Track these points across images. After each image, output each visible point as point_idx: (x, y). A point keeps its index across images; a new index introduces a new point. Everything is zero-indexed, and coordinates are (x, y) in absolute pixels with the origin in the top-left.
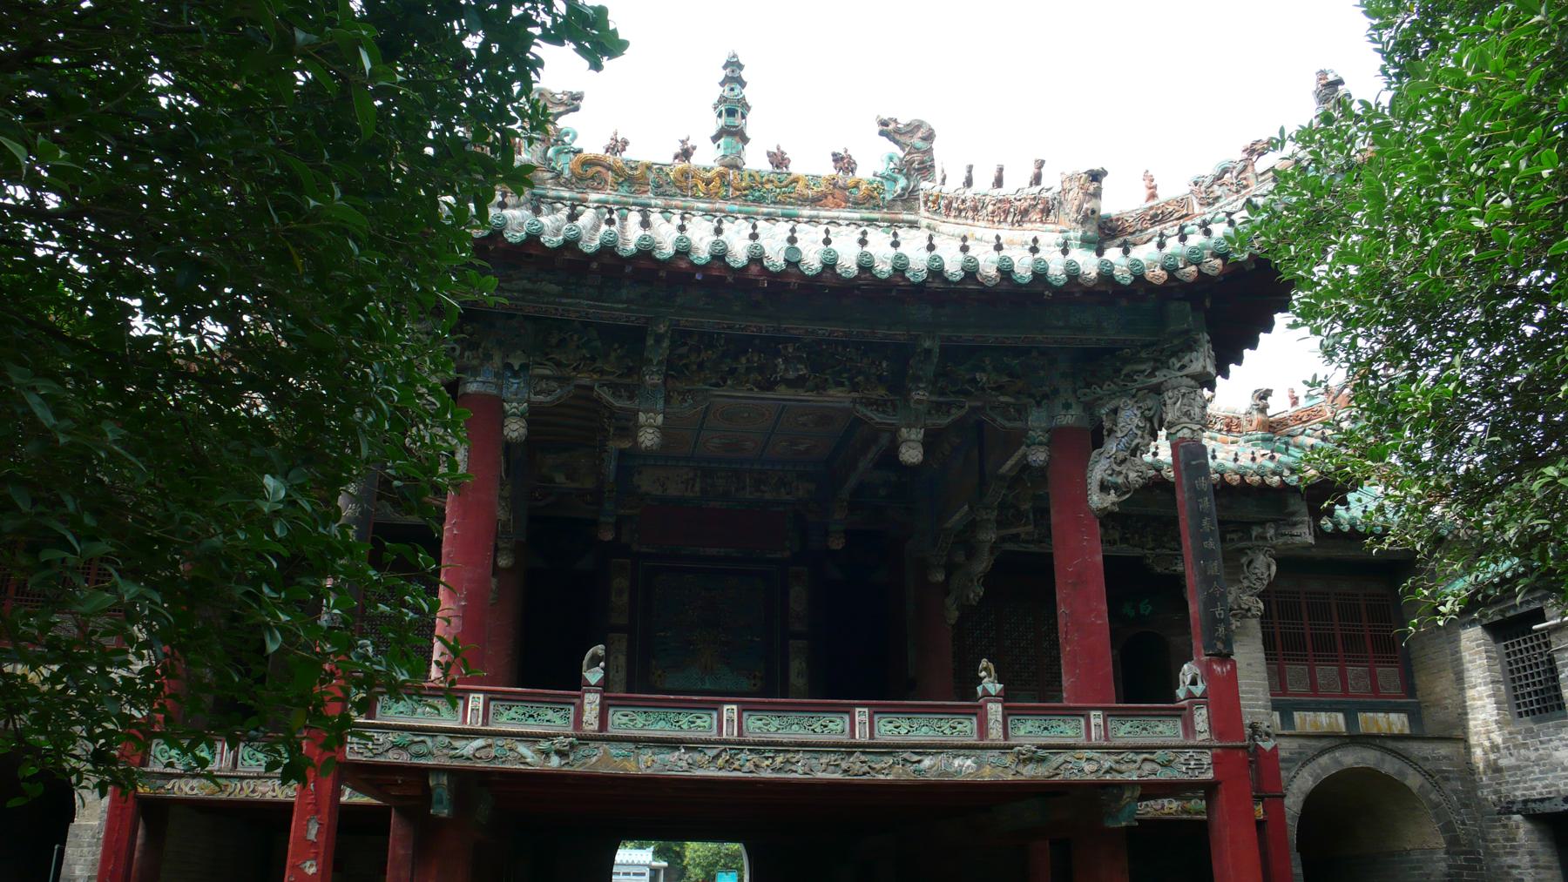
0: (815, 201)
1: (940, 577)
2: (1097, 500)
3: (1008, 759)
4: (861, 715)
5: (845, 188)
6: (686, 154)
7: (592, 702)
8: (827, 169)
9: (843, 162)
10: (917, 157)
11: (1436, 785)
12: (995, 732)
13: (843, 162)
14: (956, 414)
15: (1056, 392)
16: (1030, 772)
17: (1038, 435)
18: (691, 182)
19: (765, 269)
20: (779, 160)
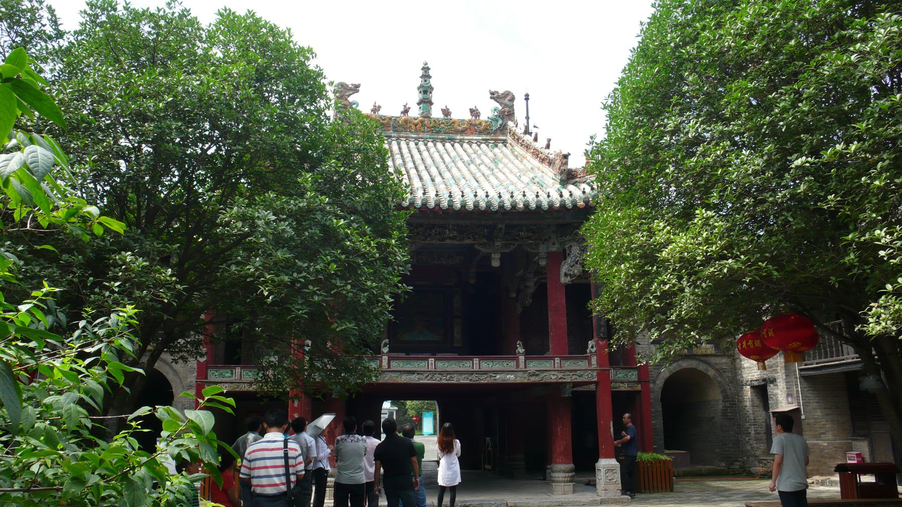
0: (462, 132)
1: (514, 295)
2: (564, 280)
3: (526, 375)
4: (476, 361)
5: (475, 125)
6: (406, 111)
7: (385, 359)
8: (468, 116)
9: (474, 112)
10: (507, 109)
11: (721, 375)
12: (522, 365)
13: (474, 112)
14: (512, 247)
15: (550, 238)
16: (533, 379)
17: (543, 255)
18: (409, 125)
19: (441, 208)
20: (446, 112)
